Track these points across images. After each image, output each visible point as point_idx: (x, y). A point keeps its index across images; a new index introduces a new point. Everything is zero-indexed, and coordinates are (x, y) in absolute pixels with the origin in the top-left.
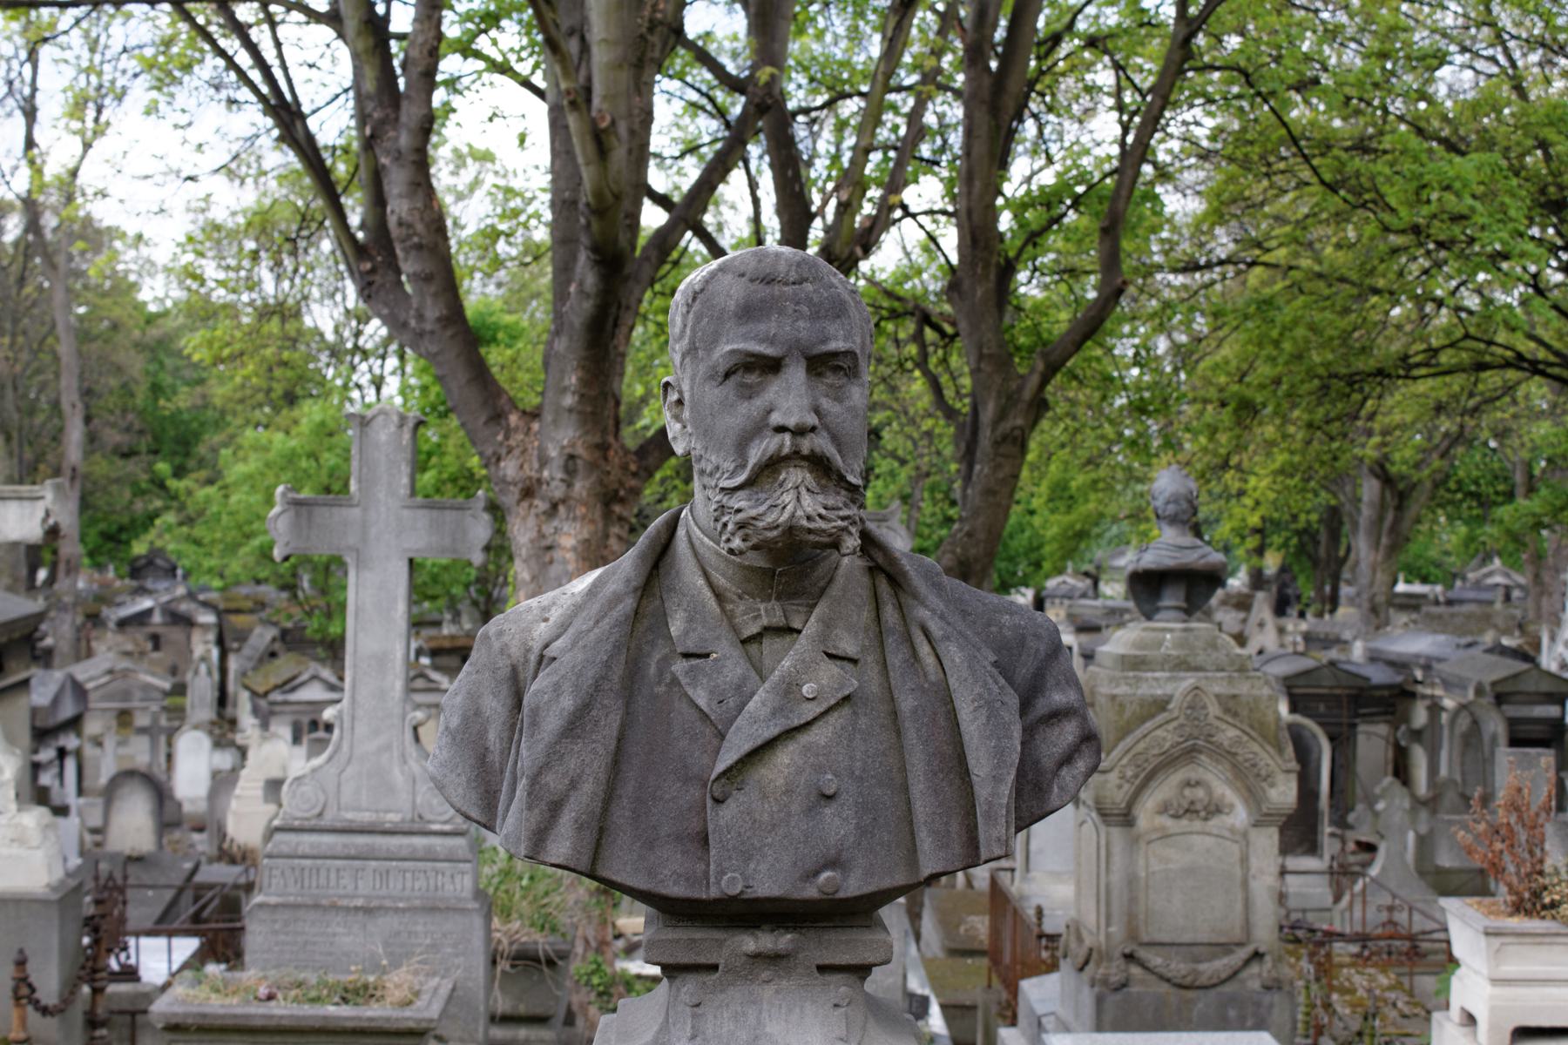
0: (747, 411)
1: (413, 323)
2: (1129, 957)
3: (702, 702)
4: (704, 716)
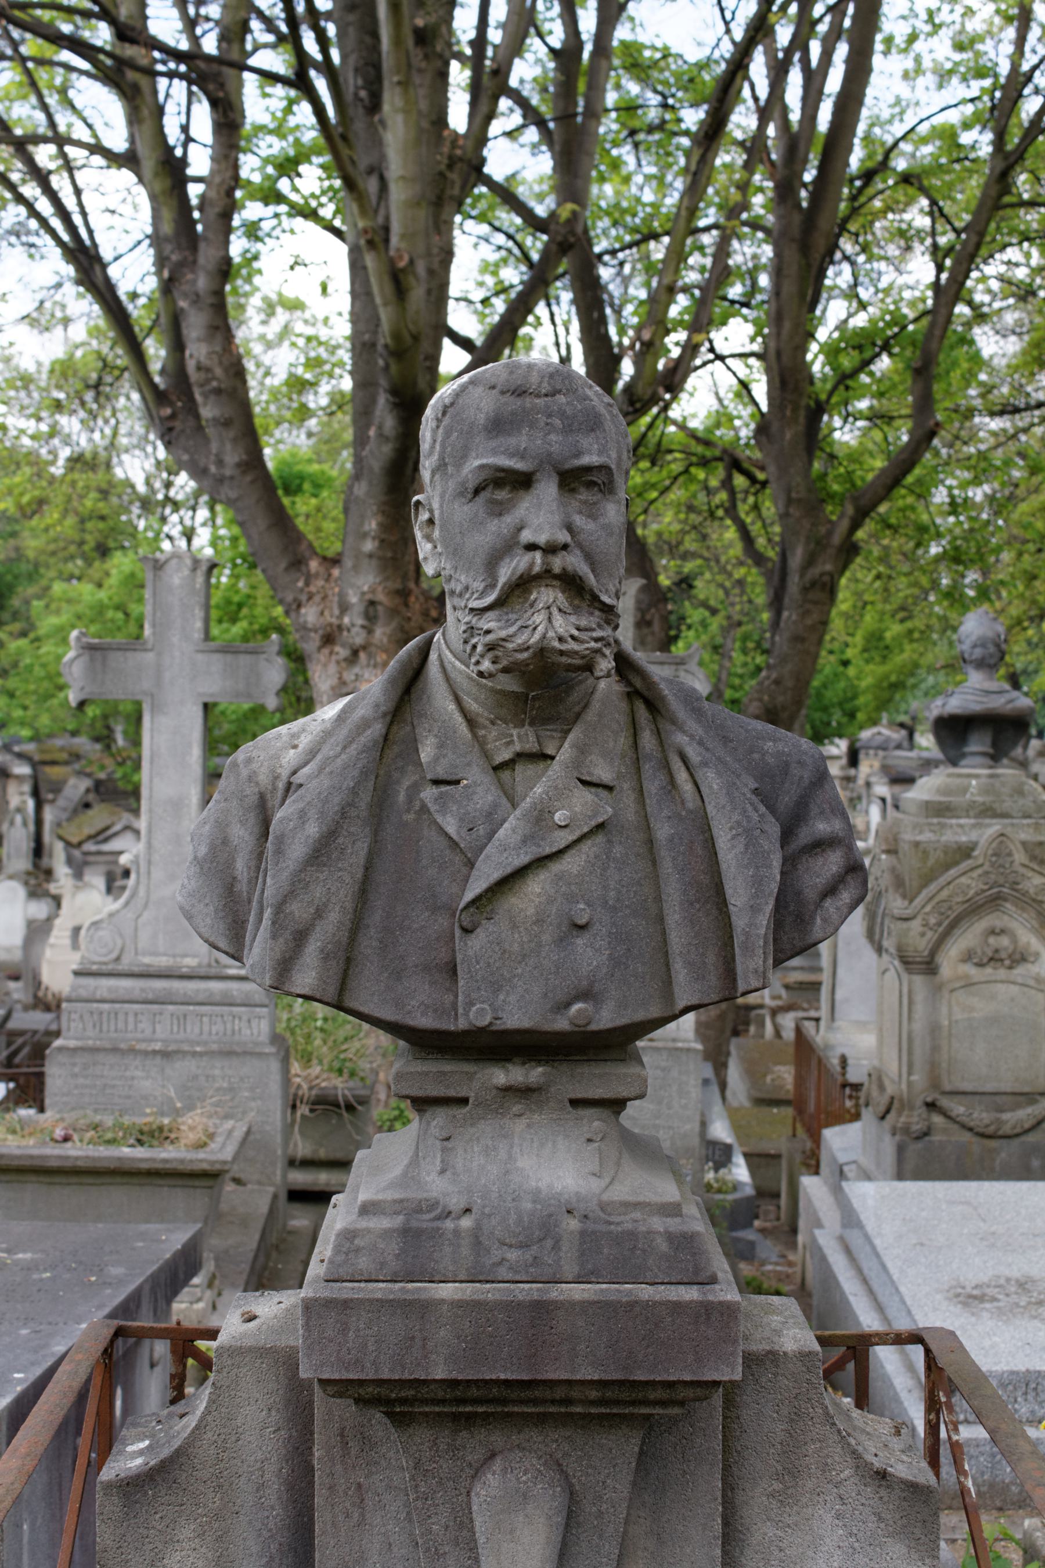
0: (497, 528)
1: (213, 469)
2: (931, 1106)
3: (451, 830)
4: (454, 844)
